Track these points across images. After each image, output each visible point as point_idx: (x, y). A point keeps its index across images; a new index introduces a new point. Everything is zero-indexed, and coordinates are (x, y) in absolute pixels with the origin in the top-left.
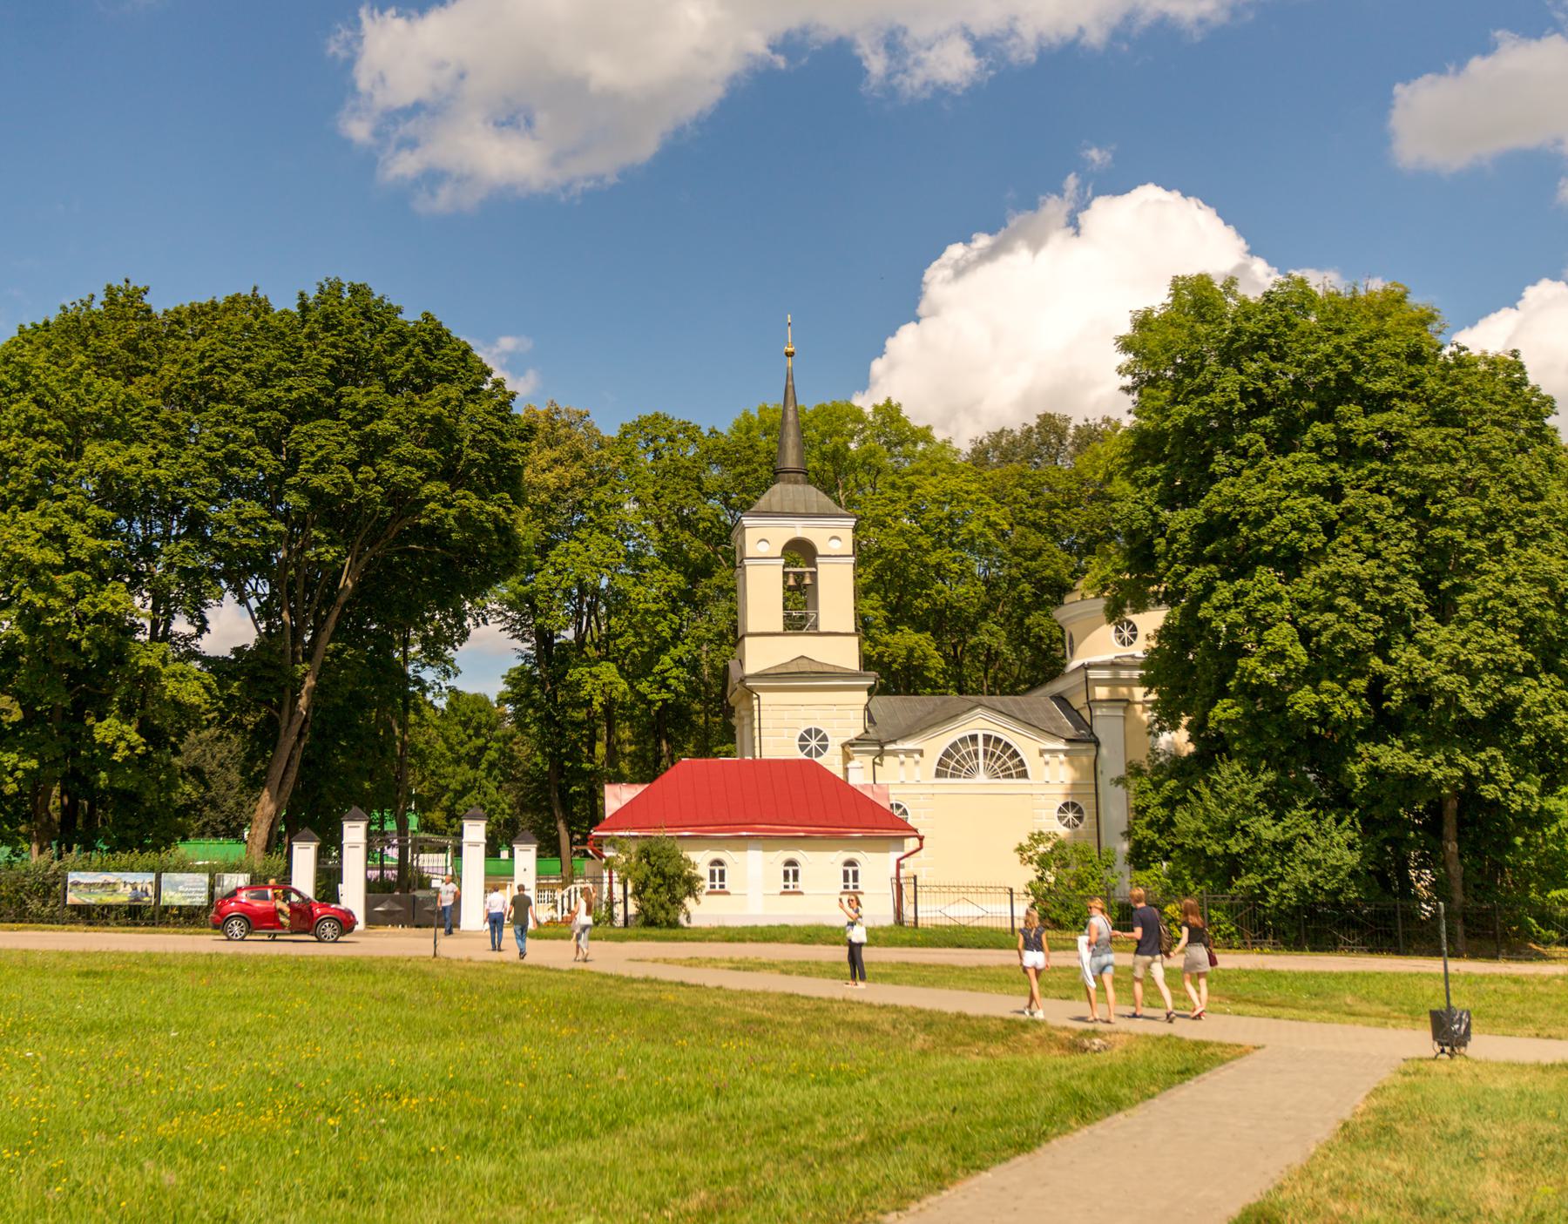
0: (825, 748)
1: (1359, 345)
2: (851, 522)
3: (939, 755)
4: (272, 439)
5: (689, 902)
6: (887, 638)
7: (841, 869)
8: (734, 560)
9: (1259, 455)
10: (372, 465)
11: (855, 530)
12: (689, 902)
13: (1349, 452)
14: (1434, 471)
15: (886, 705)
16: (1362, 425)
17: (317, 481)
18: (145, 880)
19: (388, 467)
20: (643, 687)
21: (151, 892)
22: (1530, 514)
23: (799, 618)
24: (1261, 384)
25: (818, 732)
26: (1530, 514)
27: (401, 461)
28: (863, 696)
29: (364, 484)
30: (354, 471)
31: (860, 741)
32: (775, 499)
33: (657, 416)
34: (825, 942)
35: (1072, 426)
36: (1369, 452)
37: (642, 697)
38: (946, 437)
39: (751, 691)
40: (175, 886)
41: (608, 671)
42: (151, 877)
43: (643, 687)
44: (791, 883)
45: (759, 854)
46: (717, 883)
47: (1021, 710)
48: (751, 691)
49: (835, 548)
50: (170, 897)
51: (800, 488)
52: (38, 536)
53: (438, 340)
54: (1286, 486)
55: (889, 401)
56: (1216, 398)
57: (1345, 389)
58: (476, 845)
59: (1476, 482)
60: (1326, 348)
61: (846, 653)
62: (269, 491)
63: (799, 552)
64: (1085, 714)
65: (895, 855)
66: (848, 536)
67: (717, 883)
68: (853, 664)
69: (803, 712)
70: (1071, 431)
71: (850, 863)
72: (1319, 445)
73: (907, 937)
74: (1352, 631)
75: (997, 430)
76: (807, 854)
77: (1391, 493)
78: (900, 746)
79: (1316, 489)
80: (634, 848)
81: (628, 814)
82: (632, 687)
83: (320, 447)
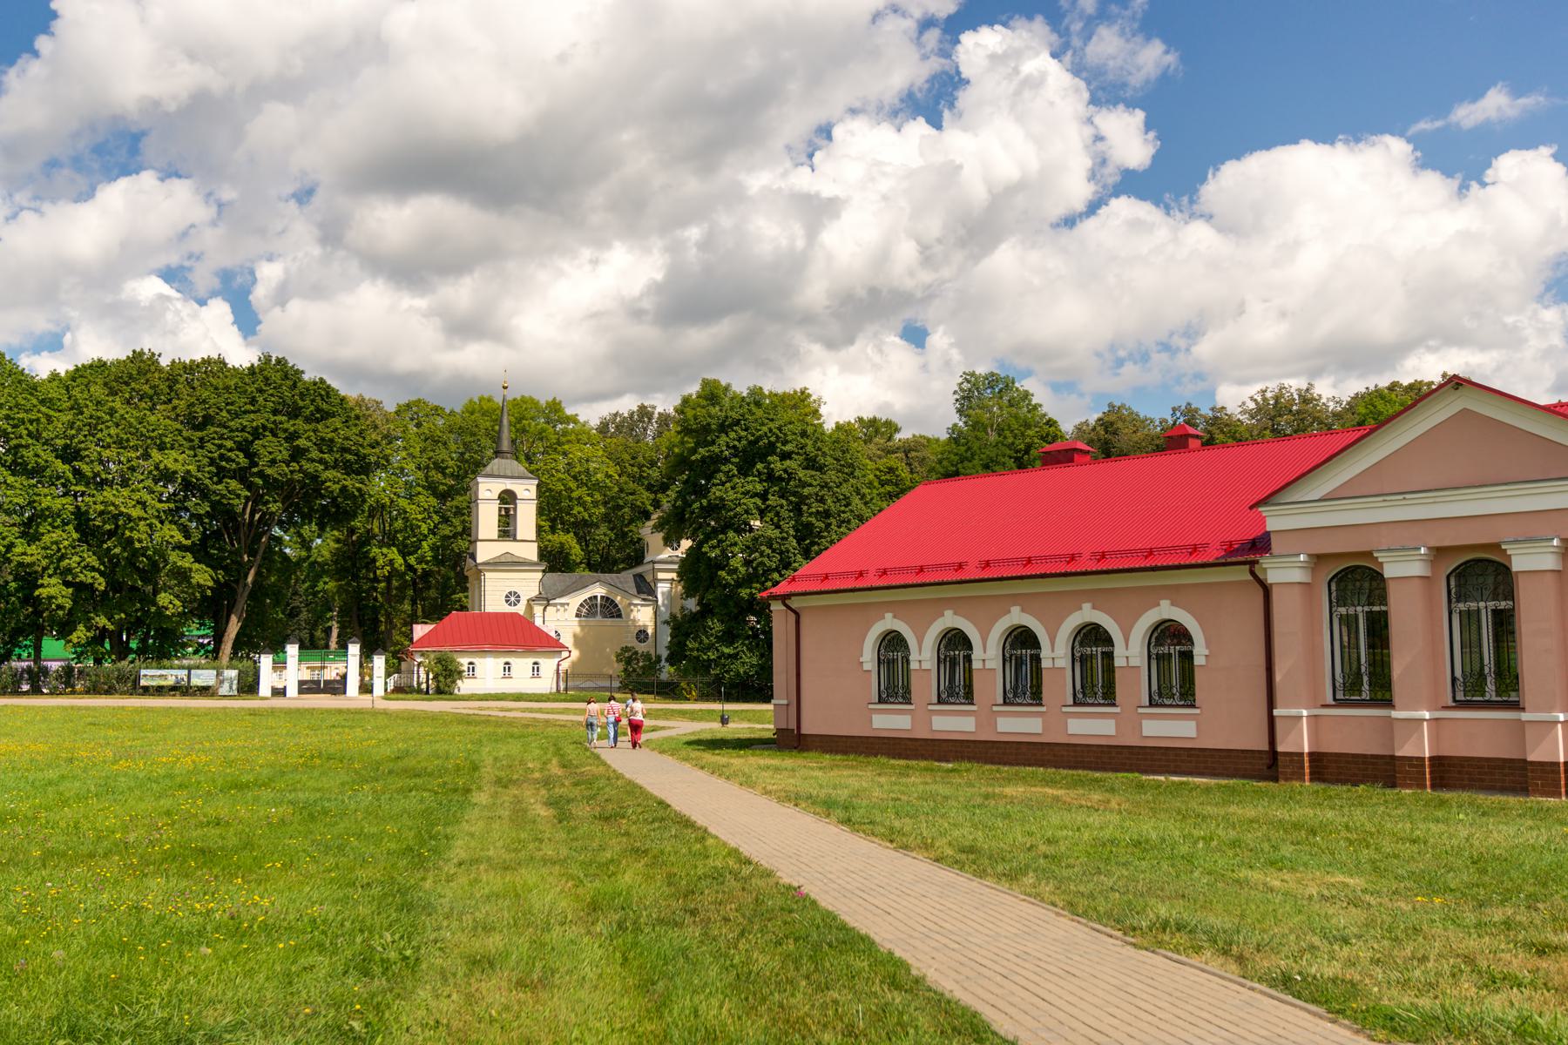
0: (519, 601)
1: (780, 429)
2: (536, 482)
3: (578, 606)
4: (244, 447)
5: (459, 682)
6: (550, 537)
7: (503, 666)
8: (473, 503)
9: (733, 476)
10: (298, 463)
11: (538, 486)
12: (459, 682)
13: (771, 477)
14: (806, 491)
15: (554, 577)
16: (777, 465)
17: (269, 471)
18: (183, 674)
19: (307, 466)
20: (412, 560)
21: (186, 679)
22: (844, 512)
23: (507, 529)
24: (736, 443)
25: (515, 593)
26: (844, 512)
27: (313, 461)
28: (540, 575)
29: (292, 472)
30: (288, 466)
31: (538, 598)
32: (495, 468)
33: (419, 401)
34: (526, 701)
35: (656, 412)
36: (780, 479)
37: (410, 567)
38: (586, 419)
39: (480, 571)
40: (198, 676)
41: (393, 553)
42: (186, 672)
43: (412, 560)
44: (507, 673)
45: (492, 659)
46: (471, 673)
47: (621, 582)
48: (480, 571)
49: (526, 495)
50: (196, 681)
51: (509, 461)
52: (134, 503)
53: (328, 393)
54: (743, 493)
55: (555, 399)
56: (715, 449)
57: (771, 448)
58: (355, 655)
59: (822, 497)
60: (765, 429)
61: (530, 552)
62: (242, 475)
63: (508, 498)
64: (652, 585)
65: (557, 660)
66: (533, 489)
67: (471, 673)
68: (534, 557)
69: (508, 583)
70: (656, 415)
71: (535, 663)
72: (760, 473)
73: (563, 697)
74: (766, 560)
75: (614, 412)
76: (545, 660)
77: (787, 500)
78: (557, 601)
79: (756, 495)
80: (432, 656)
81: (426, 639)
82: (405, 561)
83: (270, 453)
